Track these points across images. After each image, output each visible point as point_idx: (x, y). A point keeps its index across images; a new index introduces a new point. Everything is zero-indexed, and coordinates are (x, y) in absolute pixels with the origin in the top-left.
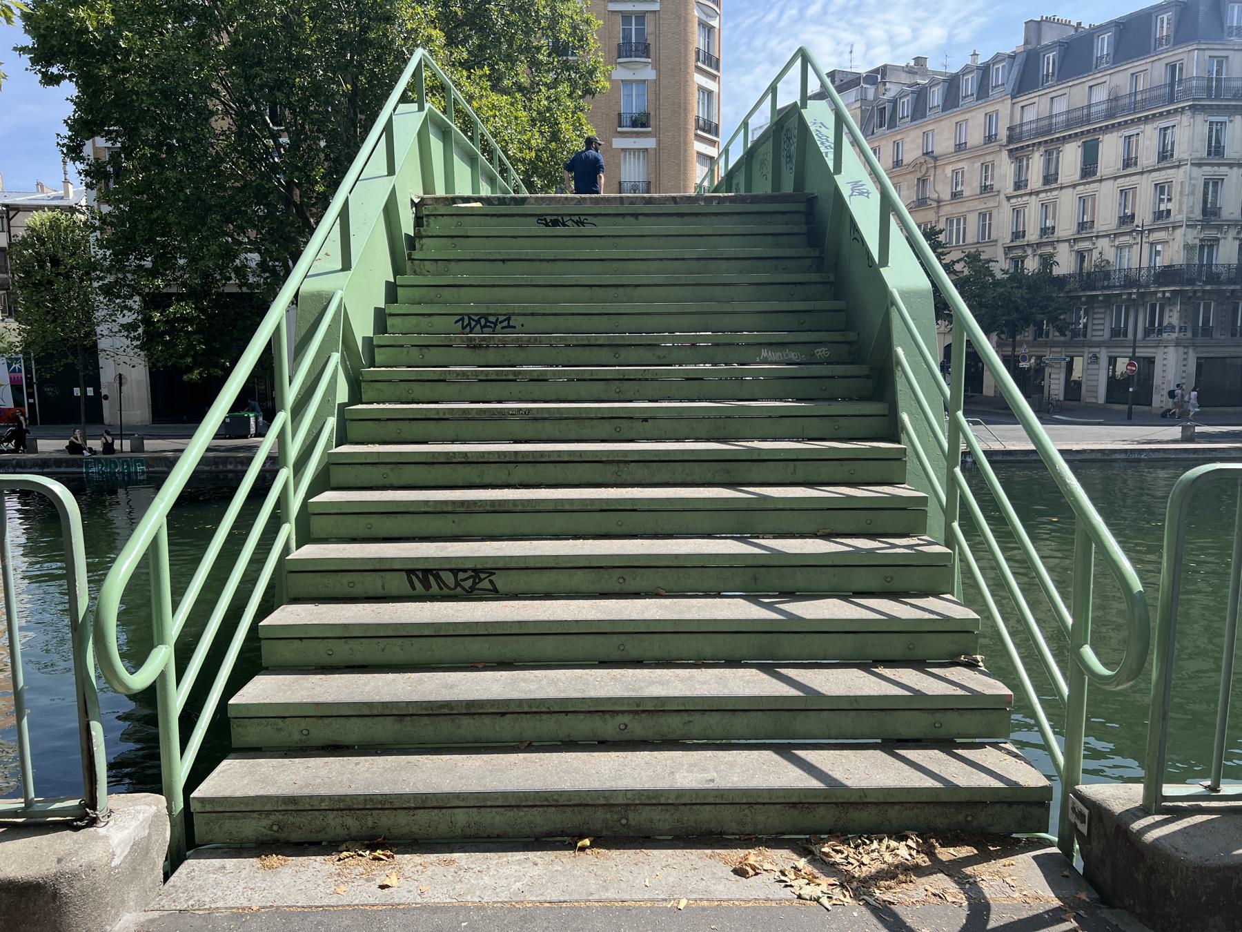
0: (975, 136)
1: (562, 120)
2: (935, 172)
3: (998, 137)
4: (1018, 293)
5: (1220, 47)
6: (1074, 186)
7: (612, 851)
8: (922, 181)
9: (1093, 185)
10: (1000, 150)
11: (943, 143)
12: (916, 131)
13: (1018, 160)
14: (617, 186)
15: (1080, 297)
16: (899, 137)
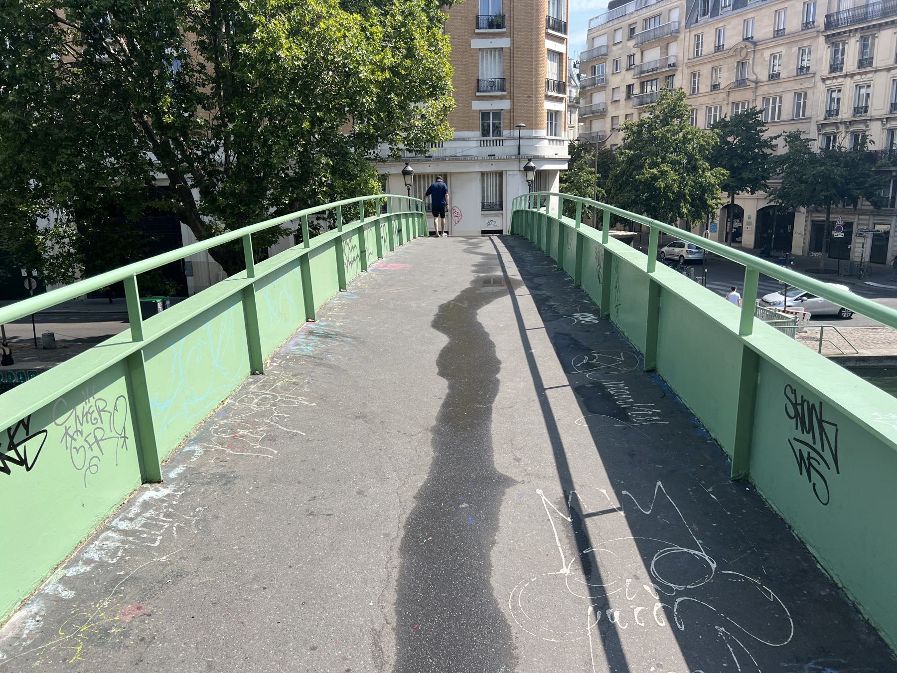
1: (417, 36)
2: (754, 55)
3: (815, 24)
4: (838, 171)
6: (889, 70)
7: (487, 330)
8: (742, 64)
10: (818, 36)
11: (763, 29)
12: (738, 19)
13: (836, 45)
14: (475, 82)
15: (891, 171)
16: (721, 25)
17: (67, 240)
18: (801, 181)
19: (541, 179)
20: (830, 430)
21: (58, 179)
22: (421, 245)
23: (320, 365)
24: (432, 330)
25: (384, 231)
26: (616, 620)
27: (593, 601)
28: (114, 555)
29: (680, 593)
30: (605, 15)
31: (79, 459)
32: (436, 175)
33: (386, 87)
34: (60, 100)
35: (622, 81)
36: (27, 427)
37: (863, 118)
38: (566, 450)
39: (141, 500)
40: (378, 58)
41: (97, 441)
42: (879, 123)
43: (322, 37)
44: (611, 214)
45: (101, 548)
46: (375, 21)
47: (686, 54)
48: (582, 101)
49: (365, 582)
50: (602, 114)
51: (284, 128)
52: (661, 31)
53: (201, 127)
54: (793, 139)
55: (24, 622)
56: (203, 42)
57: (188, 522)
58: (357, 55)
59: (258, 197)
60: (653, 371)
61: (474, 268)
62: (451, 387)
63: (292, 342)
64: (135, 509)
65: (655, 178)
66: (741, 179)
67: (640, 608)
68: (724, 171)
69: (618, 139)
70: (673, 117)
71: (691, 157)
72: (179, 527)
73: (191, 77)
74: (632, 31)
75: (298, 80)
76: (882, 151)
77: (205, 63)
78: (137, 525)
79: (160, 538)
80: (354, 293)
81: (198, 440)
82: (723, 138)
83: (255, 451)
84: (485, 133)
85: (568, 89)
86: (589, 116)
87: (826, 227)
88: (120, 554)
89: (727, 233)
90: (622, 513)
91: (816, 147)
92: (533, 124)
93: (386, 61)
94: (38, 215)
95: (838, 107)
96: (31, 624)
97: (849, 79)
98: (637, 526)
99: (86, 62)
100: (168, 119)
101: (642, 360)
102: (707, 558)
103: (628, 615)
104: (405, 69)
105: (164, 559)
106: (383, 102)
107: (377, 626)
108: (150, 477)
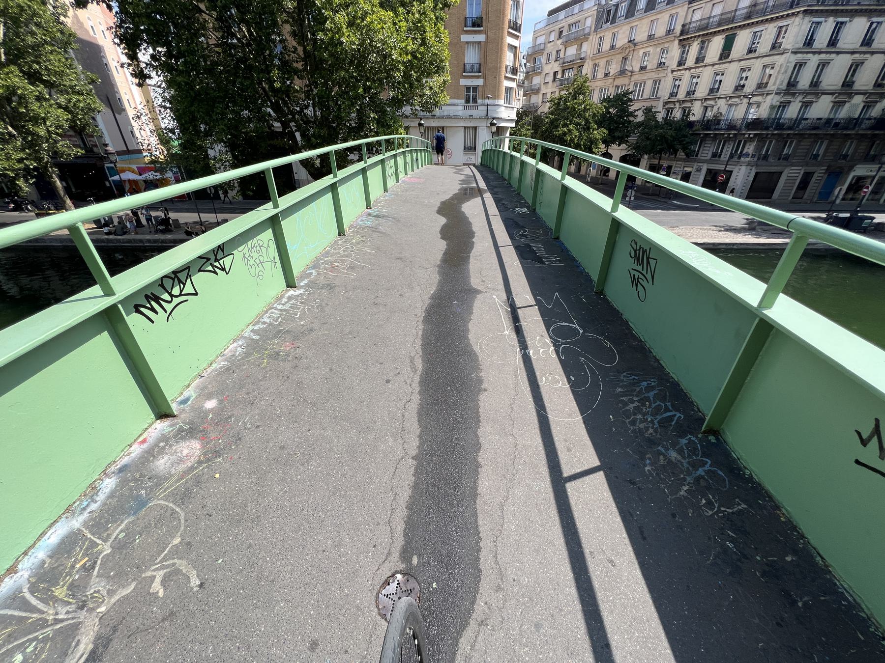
1: (428, 30)
4: (671, 132)
6: (713, 65)
8: (625, 59)
10: (674, 40)
11: (641, 35)
13: (684, 46)
14: (463, 66)
15: (700, 134)
17: (227, 163)
18: (648, 138)
19: (500, 131)
20: (652, 262)
21: (217, 124)
22: (429, 169)
23: (376, 232)
24: (437, 215)
25: (408, 159)
26: (531, 354)
27: (520, 346)
28: (277, 320)
29: (563, 343)
30: (546, 21)
31: (252, 271)
32: (438, 128)
33: (409, 66)
34: (210, 71)
35: (551, 69)
36: (223, 251)
37: (691, 99)
38: (509, 277)
39: (287, 295)
40: (404, 45)
41: (261, 263)
42: (700, 102)
43: (369, 27)
44: (542, 146)
45: (270, 317)
46: (401, 18)
47: (592, 51)
48: (526, 82)
49: (405, 335)
50: (537, 91)
51: (347, 93)
52: (579, 33)
53: (297, 91)
54: (648, 111)
55: (236, 348)
56: (294, 31)
57: (313, 307)
58: (391, 42)
59: (334, 139)
60: (558, 238)
61: (460, 182)
62: (447, 245)
63: (359, 220)
64: (284, 300)
65: (565, 134)
66: (614, 136)
67: (543, 349)
68: (605, 131)
69: (545, 108)
70: (579, 94)
71: (587, 121)
72: (308, 309)
73: (289, 55)
74: (561, 32)
75: (355, 60)
76: (698, 121)
77: (297, 46)
78: (287, 307)
79: (299, 313)
80: (393, 194)
81: (314, 267)
82: (607, 109)
83: (344, 274)
84: (468, 101)
85: (518, 74)
86: (530, 92)
87: (657, 168)
88: (280, 320)
89: (601, 171)
90: (537, 307)
91: (660, 117)
92: (496, 96)
93: (409, 47)
94: (208, 148)
95: (677, 91)
96: (240, 350)
97: (688, 71)
98: (544, 313)
99: (224, 45)
100: (277, 85)
101: (551, 233)
102: (578, 328)
103: (537, 352)
104: (421, 53)
105: (302, 323)
106: (407, 76)
107: (412, 355)
108: (290, 285)
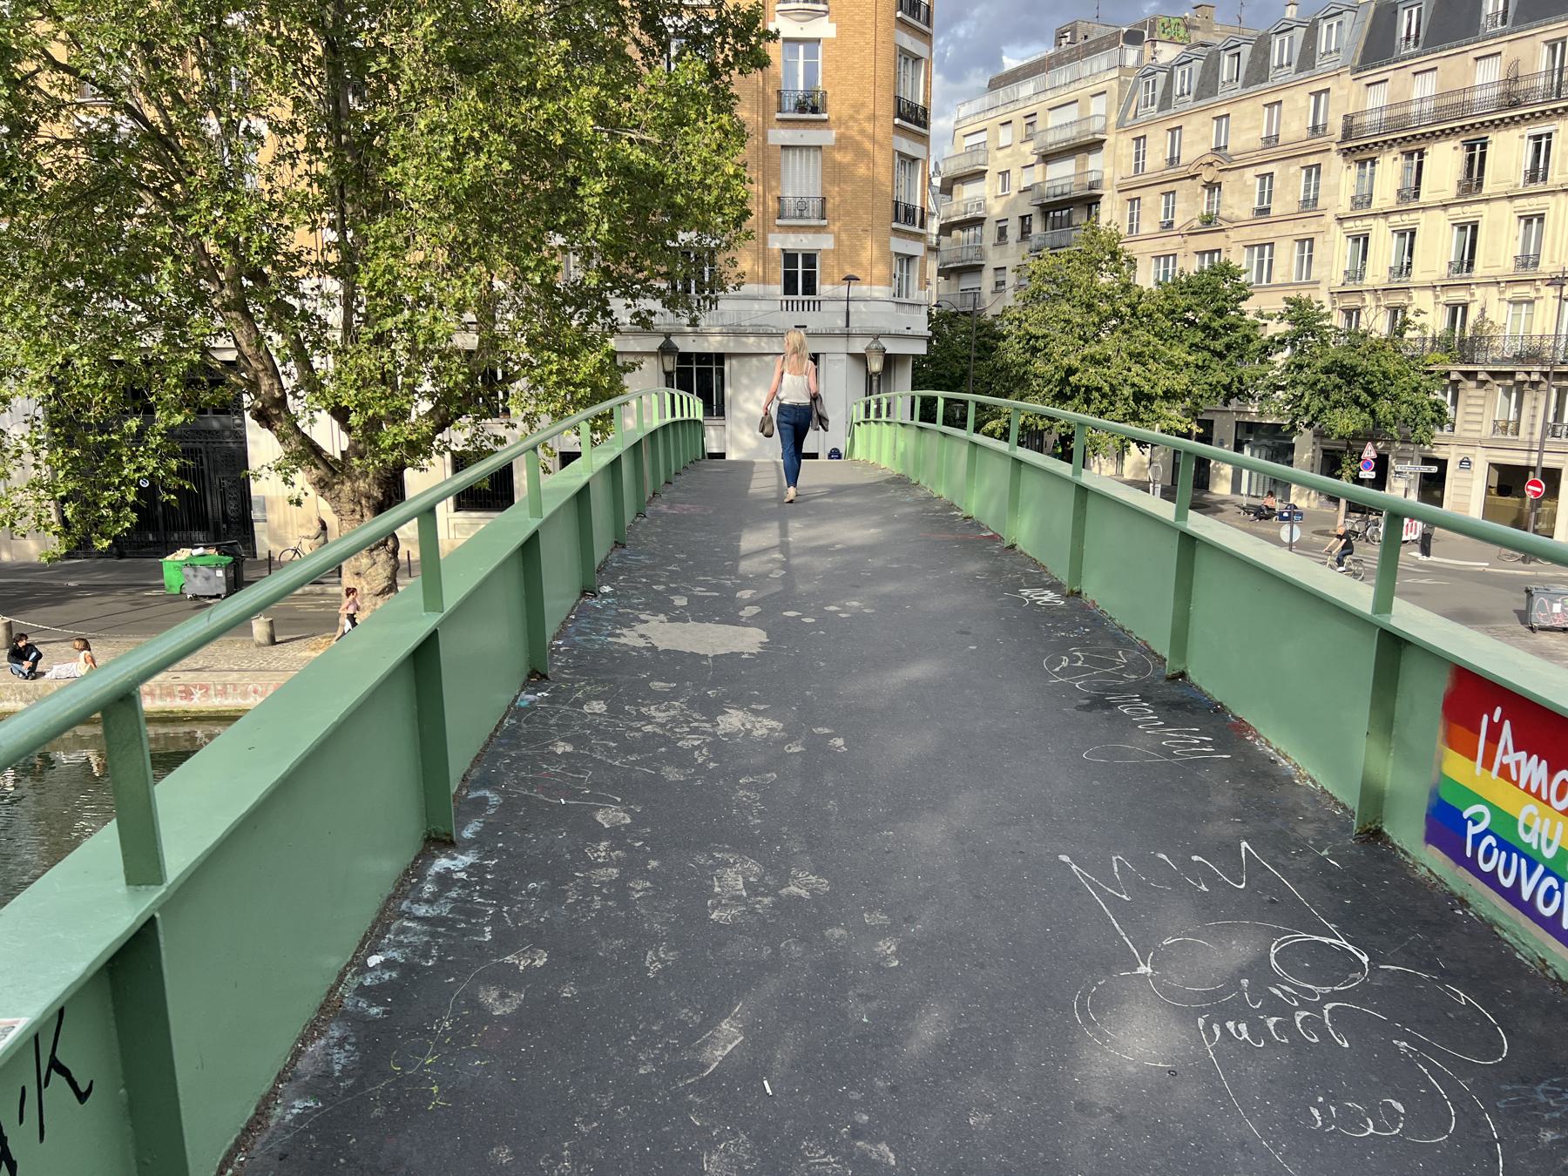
0: (1294, 126)
5: (1454, 51)
9: (1475, 207)
29: (1327, 998)
42: (1429, 293)
78: (444, 910)
84: (790, 287)
96: (340, 1058)
97: (1381, 221)
102: (1350, 948)
